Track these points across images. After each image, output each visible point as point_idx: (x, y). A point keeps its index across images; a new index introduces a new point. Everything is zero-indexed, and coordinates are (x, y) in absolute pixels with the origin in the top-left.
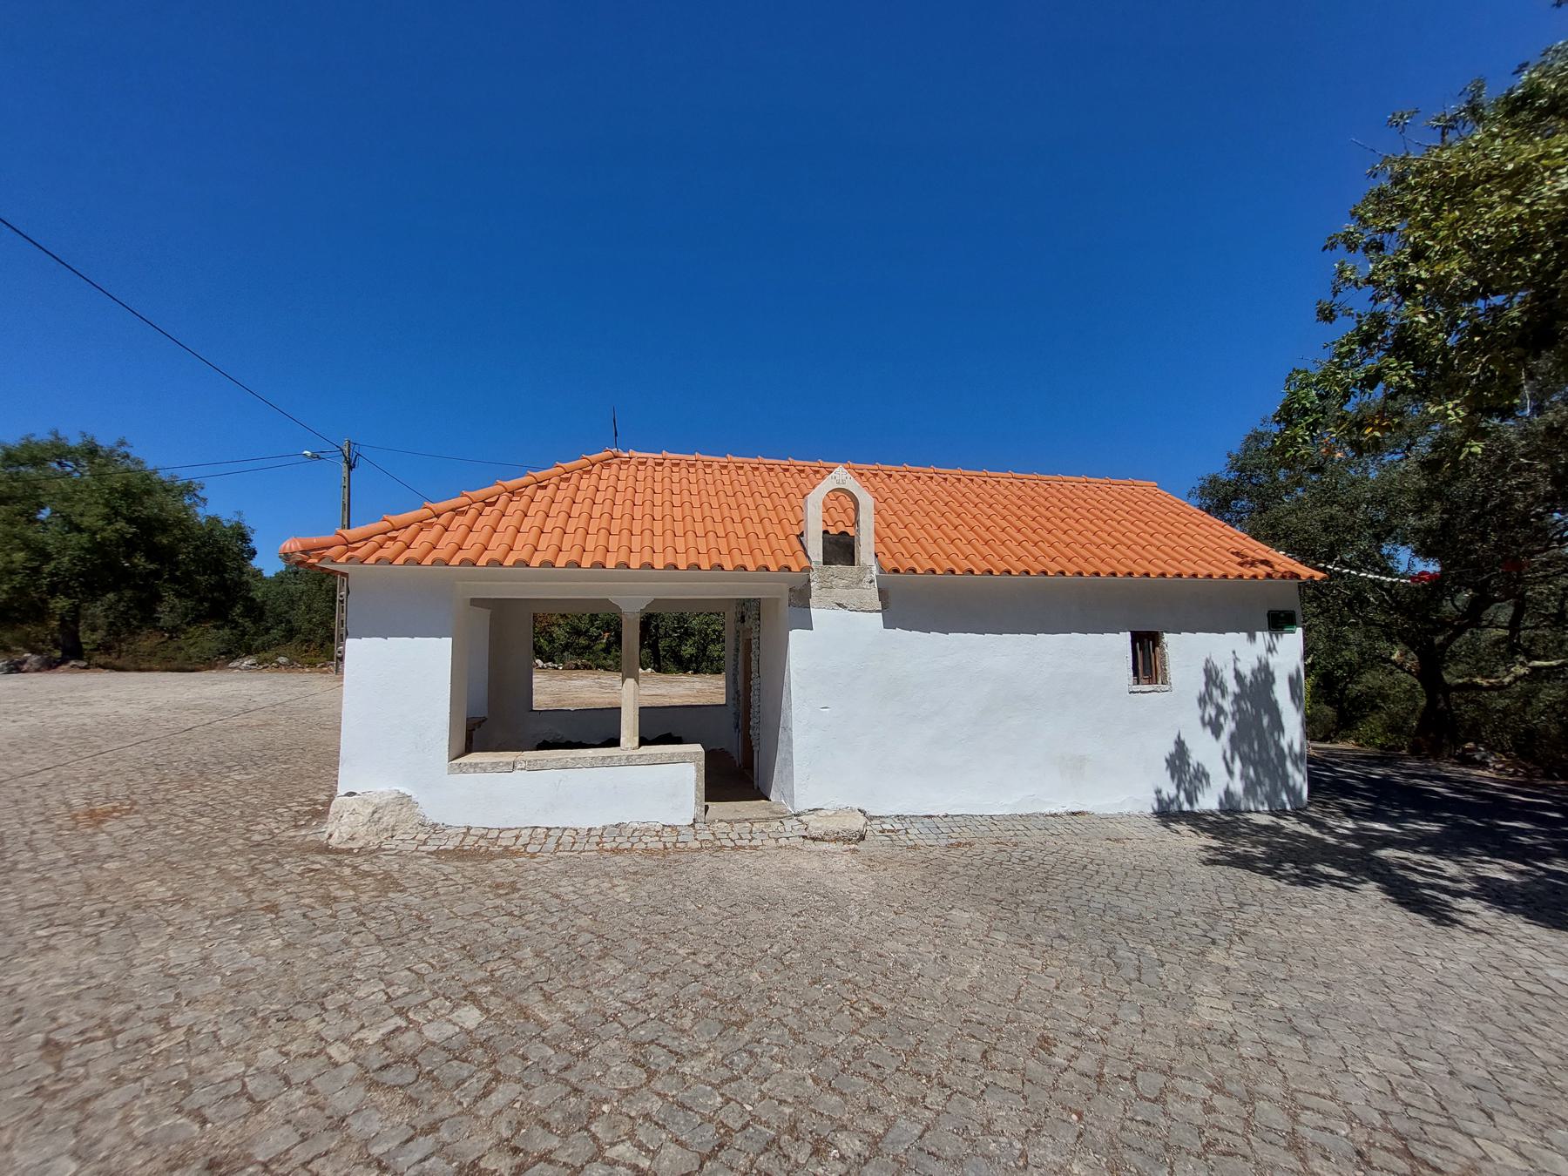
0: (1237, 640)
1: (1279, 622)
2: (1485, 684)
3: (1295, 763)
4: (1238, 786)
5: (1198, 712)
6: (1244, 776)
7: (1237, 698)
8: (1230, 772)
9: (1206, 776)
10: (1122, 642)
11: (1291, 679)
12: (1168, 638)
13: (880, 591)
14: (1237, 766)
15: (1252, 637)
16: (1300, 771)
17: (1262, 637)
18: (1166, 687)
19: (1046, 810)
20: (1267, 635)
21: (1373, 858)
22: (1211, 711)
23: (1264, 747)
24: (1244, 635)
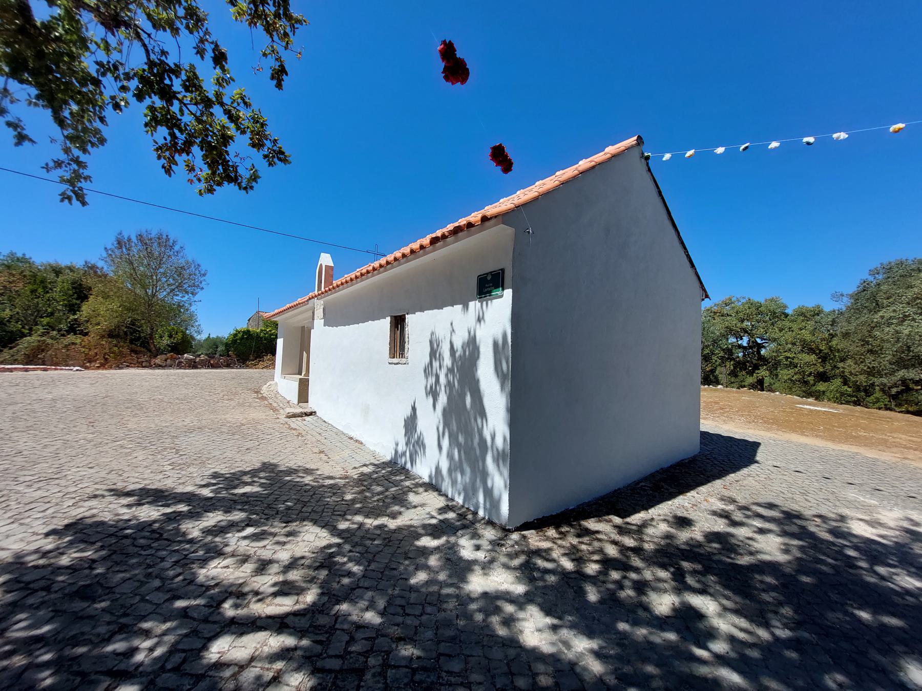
0: (453, 312)
1: (488, 285)
2: (359, 518)
3: (496, 460)
4: (445, 466)
5: (424, 382)
6: (450, 456)
7: (450, 370)
8: (440, 447)
9: (423, 446)
10: (385, 324)
11: (495, 344)
12: (409, 318)
13: (324, 310)
14: (446, 443)
15: (466, 307)
16: (501, 474)
17: (474, 305)
18: (404, 360)
19: (352, 434)
20: (478, 304)
21: (797, 581)
22: (432, 380)
23: (469, 434)
24: (459, 307)
